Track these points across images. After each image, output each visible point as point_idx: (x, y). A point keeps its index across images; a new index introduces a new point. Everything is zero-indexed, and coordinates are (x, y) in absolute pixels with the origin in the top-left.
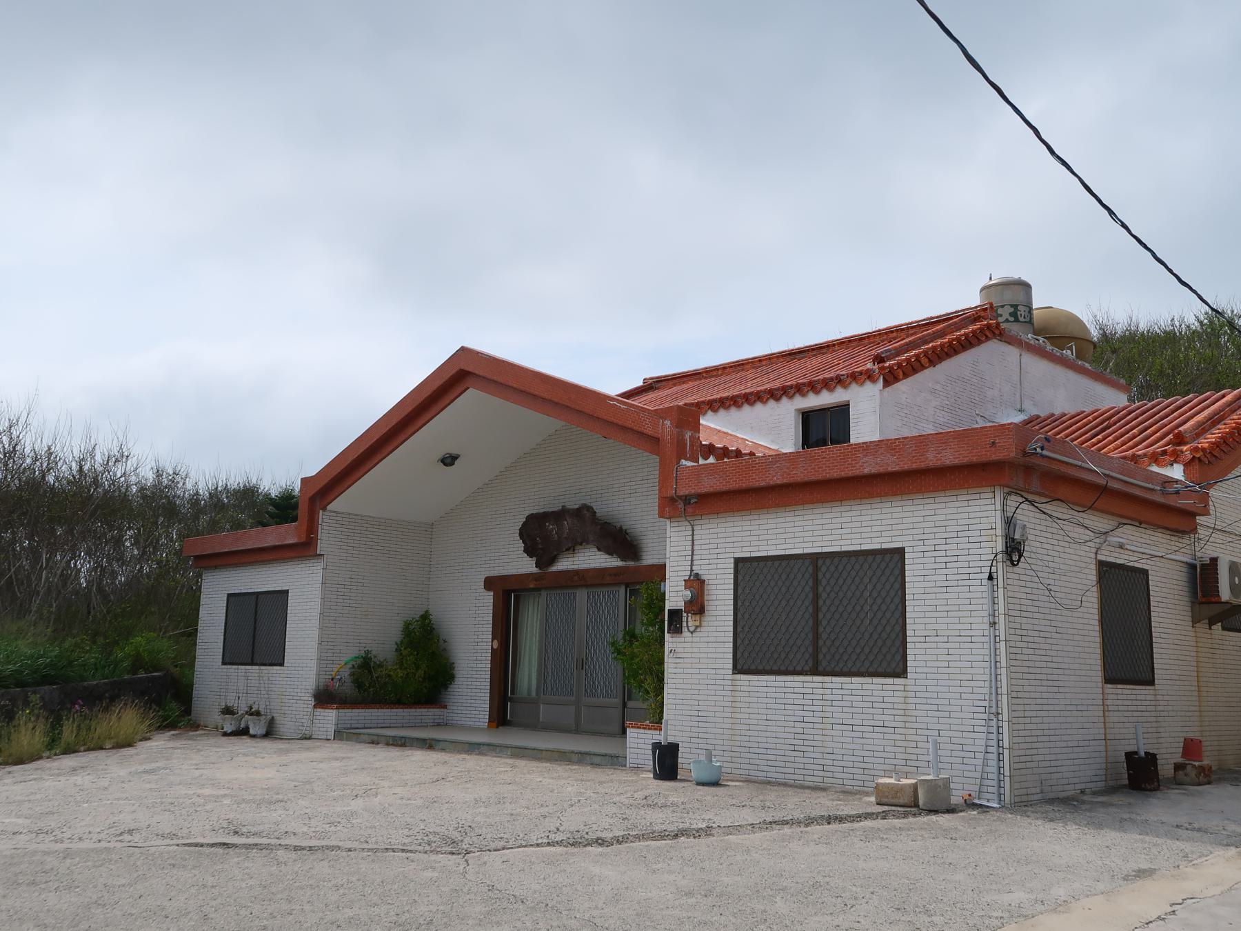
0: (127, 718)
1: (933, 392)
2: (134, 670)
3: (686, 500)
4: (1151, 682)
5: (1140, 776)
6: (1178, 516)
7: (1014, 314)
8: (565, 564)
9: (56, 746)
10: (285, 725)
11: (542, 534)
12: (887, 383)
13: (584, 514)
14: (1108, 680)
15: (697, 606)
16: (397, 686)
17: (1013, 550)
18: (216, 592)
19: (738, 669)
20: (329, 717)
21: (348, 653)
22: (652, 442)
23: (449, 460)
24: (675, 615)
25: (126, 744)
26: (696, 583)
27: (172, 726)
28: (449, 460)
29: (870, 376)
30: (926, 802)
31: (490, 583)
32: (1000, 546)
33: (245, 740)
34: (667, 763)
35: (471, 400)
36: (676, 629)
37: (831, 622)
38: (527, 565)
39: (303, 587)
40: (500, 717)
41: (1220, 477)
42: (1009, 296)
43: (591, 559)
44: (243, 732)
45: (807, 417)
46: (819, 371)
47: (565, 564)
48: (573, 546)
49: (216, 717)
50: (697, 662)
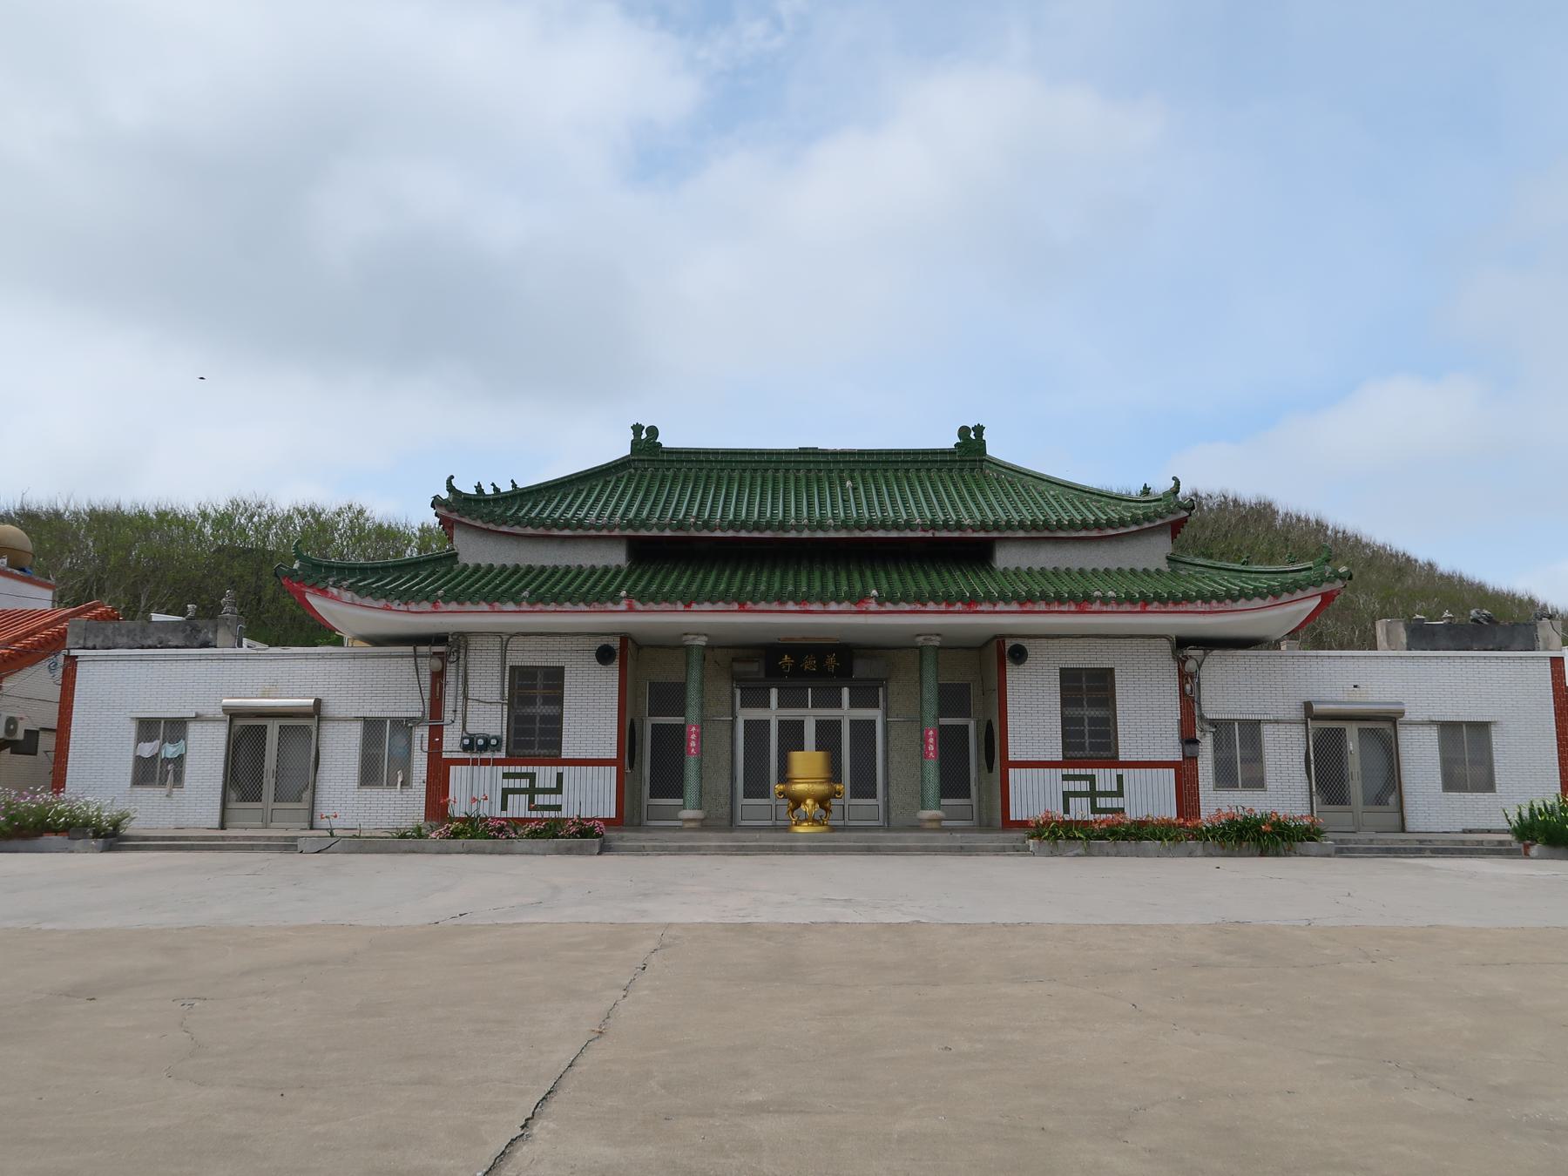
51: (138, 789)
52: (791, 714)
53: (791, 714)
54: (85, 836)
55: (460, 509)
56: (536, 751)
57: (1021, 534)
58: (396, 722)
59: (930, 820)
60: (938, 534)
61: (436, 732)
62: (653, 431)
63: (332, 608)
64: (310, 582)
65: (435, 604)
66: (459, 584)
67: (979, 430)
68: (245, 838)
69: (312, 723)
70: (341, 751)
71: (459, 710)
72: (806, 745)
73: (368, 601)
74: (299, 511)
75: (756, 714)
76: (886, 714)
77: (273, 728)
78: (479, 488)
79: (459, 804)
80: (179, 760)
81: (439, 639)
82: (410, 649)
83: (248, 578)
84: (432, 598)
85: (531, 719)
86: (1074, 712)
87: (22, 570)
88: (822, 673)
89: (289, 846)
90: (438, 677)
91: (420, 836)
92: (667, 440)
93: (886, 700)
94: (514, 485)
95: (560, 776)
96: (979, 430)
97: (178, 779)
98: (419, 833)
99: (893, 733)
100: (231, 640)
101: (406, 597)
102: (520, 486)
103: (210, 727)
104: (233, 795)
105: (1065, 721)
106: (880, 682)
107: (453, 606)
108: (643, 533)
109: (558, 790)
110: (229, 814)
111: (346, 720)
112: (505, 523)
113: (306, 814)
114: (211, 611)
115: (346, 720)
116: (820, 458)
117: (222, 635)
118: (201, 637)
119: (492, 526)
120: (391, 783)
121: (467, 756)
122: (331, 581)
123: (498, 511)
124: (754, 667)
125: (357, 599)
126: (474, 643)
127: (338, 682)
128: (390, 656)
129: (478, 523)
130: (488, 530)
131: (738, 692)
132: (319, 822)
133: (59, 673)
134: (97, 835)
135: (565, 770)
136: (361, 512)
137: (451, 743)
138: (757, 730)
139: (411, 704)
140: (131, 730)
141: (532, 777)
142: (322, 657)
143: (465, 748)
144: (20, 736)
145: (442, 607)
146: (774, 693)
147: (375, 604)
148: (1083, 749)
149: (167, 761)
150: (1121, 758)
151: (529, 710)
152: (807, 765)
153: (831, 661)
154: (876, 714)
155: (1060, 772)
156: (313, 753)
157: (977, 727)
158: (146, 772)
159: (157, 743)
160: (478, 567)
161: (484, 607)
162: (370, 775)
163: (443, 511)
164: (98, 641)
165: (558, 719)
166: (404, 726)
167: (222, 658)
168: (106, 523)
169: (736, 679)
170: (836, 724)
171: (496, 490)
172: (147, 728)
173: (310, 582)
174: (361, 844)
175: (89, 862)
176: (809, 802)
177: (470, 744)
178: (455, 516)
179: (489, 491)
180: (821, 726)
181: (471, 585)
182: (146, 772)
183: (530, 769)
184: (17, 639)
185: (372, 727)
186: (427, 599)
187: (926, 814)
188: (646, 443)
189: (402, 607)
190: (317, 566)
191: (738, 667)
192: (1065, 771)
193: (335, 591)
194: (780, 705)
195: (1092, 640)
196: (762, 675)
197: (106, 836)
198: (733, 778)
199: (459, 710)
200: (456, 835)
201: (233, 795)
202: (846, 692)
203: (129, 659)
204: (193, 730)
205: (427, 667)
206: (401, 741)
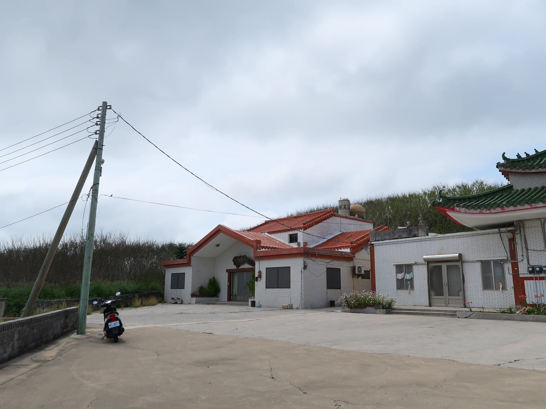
0: (153, 300)
1: (317, 230)
2: (152, 290)
3: (258, 257)
4: (340, 289)
5: (332, 304)
6: (349, 258)
7: (345, 207)
8: (241, 267)
9: (142, 305)
10: (185, 301)
11: (237, 261)
12: (304, 230)
13: (245, 257)
14: (328, 288)
15: (260, 276)
16: (208, 292)
17: (305, 267)
18: (169, 273)
19: (266, 288)
20: (194, 299)
21: (198, 286)
22: (252, 246)
23: (218, 245)
24: (257, 278)
25: (153, 305)
26: (260, 272)
27: (161, 302)
28: (218, 245)
29: (301, 228)
30: (290, 307)
31: (227, 271)
32: (303, 266)
33: (176, 305)
34: (253, 304)
35: (221, 235)
36: (257, 281)
37: (279, 279)
38: (234, 267)
39: (188, 272)
40: (229, 299)
41: (358, 251)
42: (344, 203)
43: (247, 266)
44: (176, 303)
45: (291, 236)
46: (296, 224)
47: (241, 267)
48: (243, 264)
49: (170, 300)
50: (260, 286)
51: (399, 291)
54: (380, 308)
55: (508, 166)
58: (496, 262)
61: (515, 266)
63: (460, 216)
64: (447, 206)
65: (502, 208)
66: (514, 198)
68: (436, 311)
69: (459, 264)
70: (473, 276)
71: (525, 255)
73: (472, 211)
74: (458, 186)
77: (444, 266)
78: (518, 156)
79: (530, 299)
80: (412, 280)
81: (511, 224)
82: (497, 230)
83: (432, 212)
84: (501, 206)
87: (363, 218)
89: (453, 315)
90: (512, 241)
91: (512, 312)
94: (536, 151)
97: (412, 287)
98: (510, 311)
100: (424, 233)
101: (489, 207)
102: (540, 151)
103: (421, 267)
104: (433, 293)
107: (512, 208)
110: (432, 301)
111: (473, 262)
112: (533, 168)
113: (462, 301)
114: (416, 223)
115: (473, 262)
117: (420, 232)
118: (413, 233)
119: (527, 171)
120: (497, 288)
121: (532, 276)
122: (455, 205)
123: (529, 164)
125: (467, 211)
126: (527, 224)
127: (470, 248)
128: (488, 234)
129: (520, 171)
130: (525, 173)
132: (467, 305)
133: (369, 250)
134: (383, 308)
136: (482, 183)
137: (523, 270)
139: (502, 254)
140: (394, 269)
142: (459, 236)
143: (530, 272)
144: (363, 272)
145: (506, 209)
147: (475, 212)
149: (409, 280)
156: (461, 277)
158: (402, 284)
159: (403, 273)
160: (523, 190)
161: (527, 206)
162: (487, 285)
163: (503, 169)
164: (380, 238)
166: (499, 263)
167: (421, 241)
168: (393, 200)
171: (527, 155)
172: (399, 268)
173: (447, 206)
174: (484, 315)
175: (381, 318)
177: (533, 270)
178: (508, 170)
179: (524, 156)
181: (520, 198)
182: (402, 284)
184: (358, 240)
185: (485, 265)
186: (498, 206)
189: (488, 212)
190: (449, 199)
193: (457, 208)
197: (386, 308)
199: (525, 255)
200: (529, 312)
201: (433, 293)
203: (390, 243)
204: (415, 268)
205: (506, 237)
206: (499, 270)
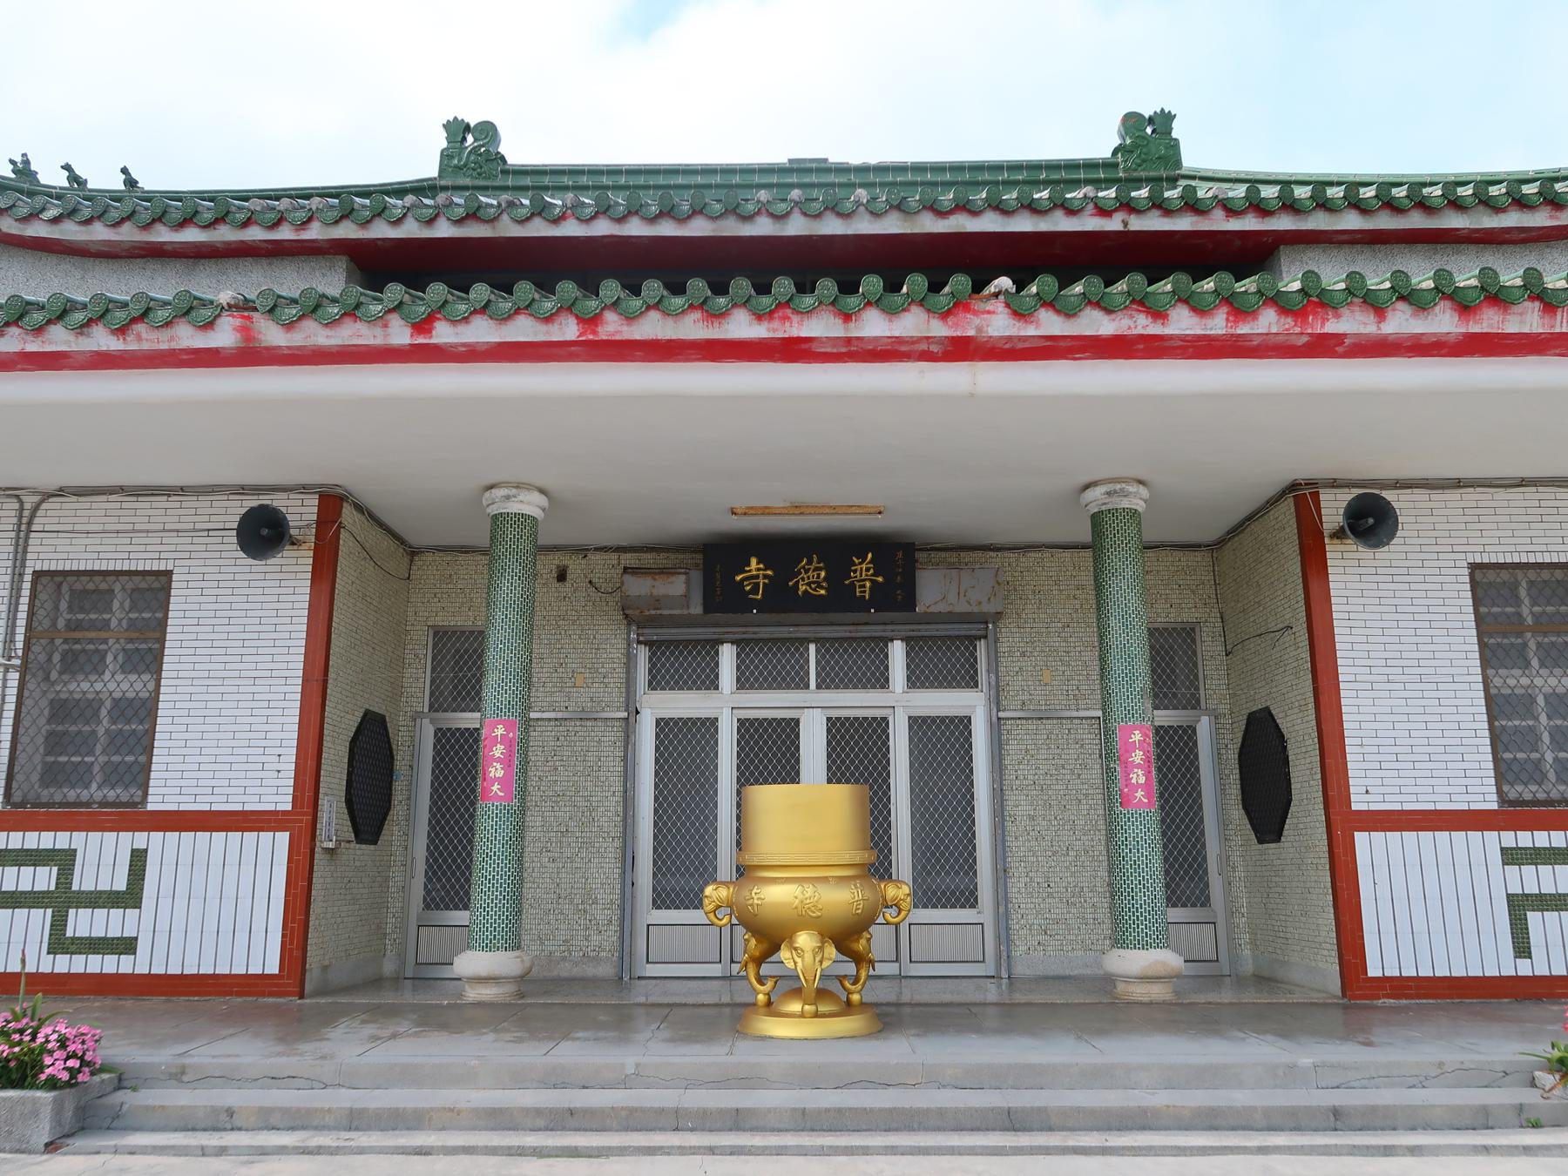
52: (770, 703)
53: (770, 703)
56: (95, 792)
57: (1352, 221)
59: (1145, 978)
60: (1138, 224)
62: (488, 131)
67: (1163, 120)
72: (489, 693)
75: (685, 704)
76: (996, 702)
85: (89, 709)
86: (1512, 680)
88: (840, 599)
92: (517, 150)
93: (994, 667)
94: (131, 183)
95: (138, 859)
96: (1163, 120)
99: (1013, 749)
102: (147, 183)
105: (1495, 705)
106: (980, 625)
108: (381, 231)
109: (130, 898)
116: (831, 178)
124: (676, 586)
131: (643, 654)
135: (153, 841)
138: (685, 744)
141: (64, 861)
146: (727, 656)
148: (1541, 779)
150: (158, 801)
151: (83, 687)
152: (798, 838)
153: (863, 572)
154: (970, 703)
155: (1495, 841)
157: (1217, 731)
165: (147, 709)
169: (638, 618)
170: (877, 728)
176: (805, 940)
180: (838, 729)
183: (61, 840)
187: (1131, 961)
188: (472, 151)
191: (638, 587)
192: (1508, 838)
194: (743, 683)
195: (1546, 492)
196: (697, 609)
198: (628, 860)
202: (897, 652)
